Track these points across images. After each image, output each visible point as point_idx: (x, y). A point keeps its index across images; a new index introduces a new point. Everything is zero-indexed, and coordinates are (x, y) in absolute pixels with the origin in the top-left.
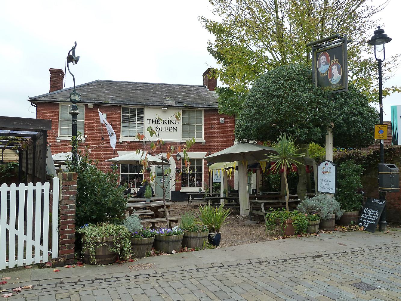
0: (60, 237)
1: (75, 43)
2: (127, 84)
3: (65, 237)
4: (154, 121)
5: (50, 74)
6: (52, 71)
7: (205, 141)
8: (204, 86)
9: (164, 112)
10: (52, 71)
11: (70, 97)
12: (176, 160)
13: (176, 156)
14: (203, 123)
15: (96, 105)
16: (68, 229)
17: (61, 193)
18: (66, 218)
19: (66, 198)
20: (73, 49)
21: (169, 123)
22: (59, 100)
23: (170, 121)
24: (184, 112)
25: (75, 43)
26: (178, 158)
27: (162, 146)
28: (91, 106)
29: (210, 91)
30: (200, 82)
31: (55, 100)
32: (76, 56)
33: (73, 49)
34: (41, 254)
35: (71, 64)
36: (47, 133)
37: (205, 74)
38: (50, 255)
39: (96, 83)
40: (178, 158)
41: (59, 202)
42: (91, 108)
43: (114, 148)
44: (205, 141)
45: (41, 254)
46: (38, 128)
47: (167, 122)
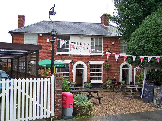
0: (55, 106)
1: (54, 5)
2: (71, 24)
3: (57, 106)
4: (75, 43)
5: (18, 18)
6: (19, 16)
7: (103, 55)
8: (102, 23)
9: (81, 38)
10: (19, 16)
11: (51, 33)
12: (87, 65)
13: (87, 63)
14: (102, 45)
15: (44, 34)
16: (59, 102)
17: (56, 83)
18: (58, 96)
19: (58, 86)
20: (53, 8)
21: (84, 44)
22: (25, 32)
23: (83, 44)
24: (92, 39)
25: (54, 5)
26: (89, 64)
27: (80, 57)
28: (41, 35)
29: (105, 27)
30: (99, 21)
31: (22, 32)
32: (54, 11)
33: (53, 8)
34: (47, 114)
35: (51, 16)
36: (38, 52)
37: (102, 18)
38: (50, 114)
39: (43, 22)
40: (89, 64)
41: (55, 88)
42: (41, 36)
43: (71, 61)
44: (103, 55)
45: (47, 114)
46: (30, 49)
47: (82, 44)
